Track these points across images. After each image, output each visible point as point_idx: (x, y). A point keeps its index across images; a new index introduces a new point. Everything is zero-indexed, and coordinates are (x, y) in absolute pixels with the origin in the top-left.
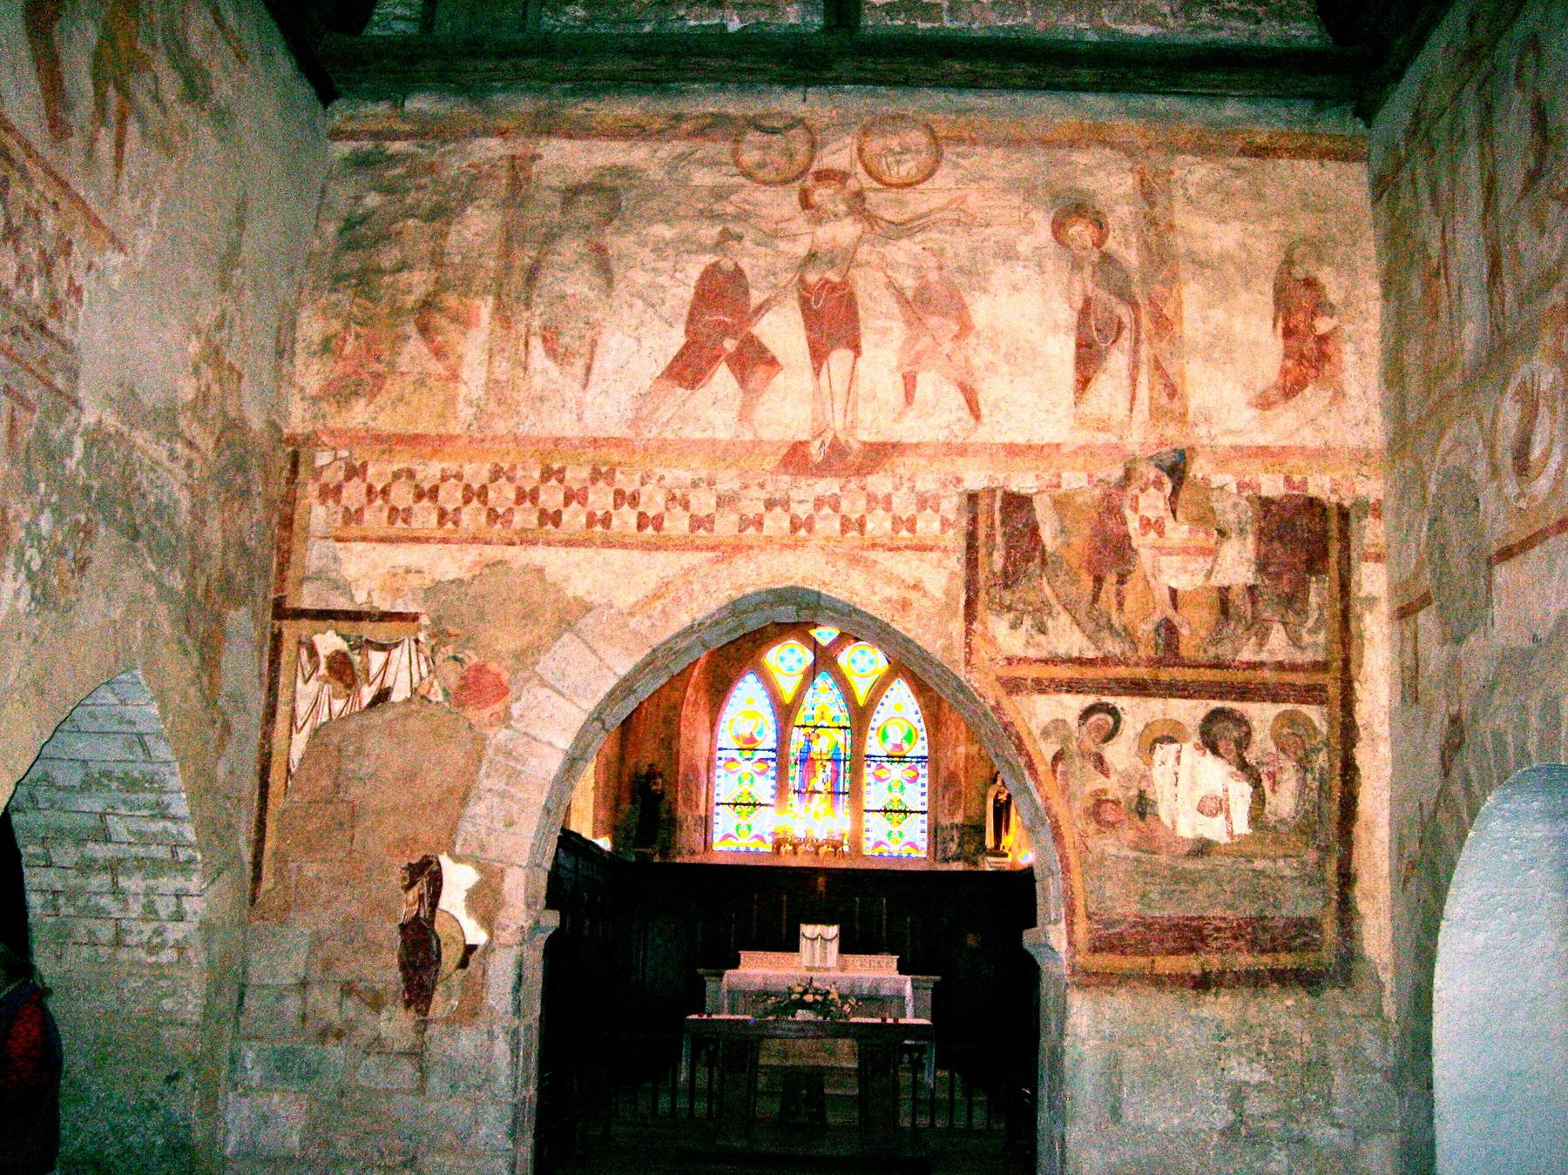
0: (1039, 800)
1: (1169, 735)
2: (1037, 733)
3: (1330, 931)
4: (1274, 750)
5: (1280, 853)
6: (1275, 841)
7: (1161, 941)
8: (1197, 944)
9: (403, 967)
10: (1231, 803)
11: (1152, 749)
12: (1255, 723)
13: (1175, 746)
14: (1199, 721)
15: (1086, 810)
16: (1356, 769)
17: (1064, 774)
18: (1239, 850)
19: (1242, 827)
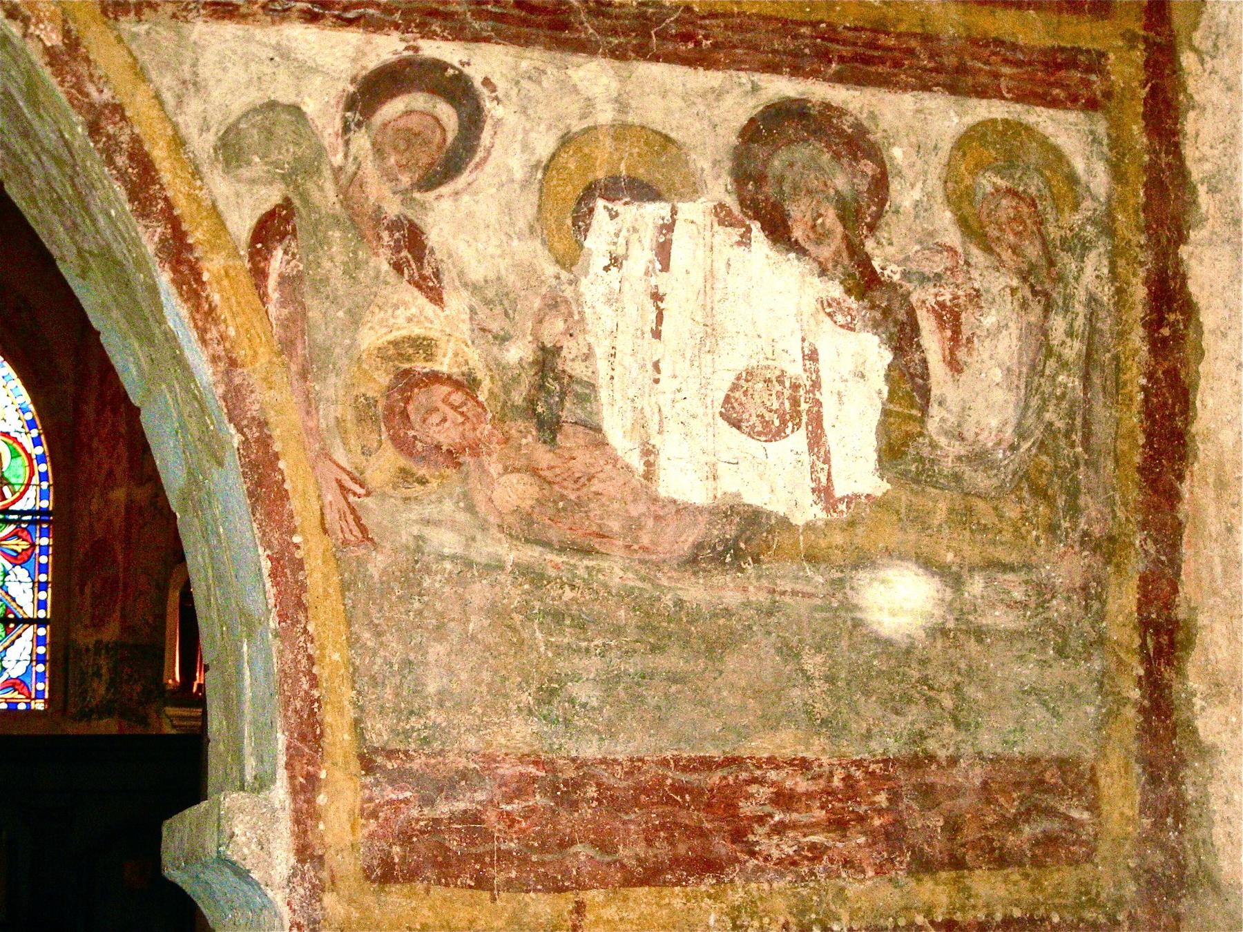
0: (205, 372)
2: (202, 144)
3: (1121, 796)
4: (953, 237)
5: (973, 554)
6: (963, 517)
7: (604, 845)
8: (721, 847)
10: (826, 397)
11: (582, 218)
13: (655, 211)
15: (364, 412)
16: (1189, 308)
17: (289, 282)
19: (858, 471)
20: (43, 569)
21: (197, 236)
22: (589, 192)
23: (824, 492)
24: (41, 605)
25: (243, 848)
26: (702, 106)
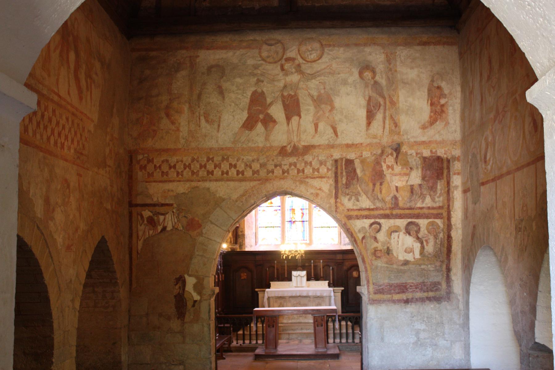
1: (396, 230)
2: (357, 231)
3: (444, 285)
4: (427, 233)
6: (428, 259)
8: (405, 290)
9: (176, 308)
11: (391, 234)
12: (421, 226)
13: (397, 233)
14: (405, 225)
16: (451, 238)
18: (417, 263)
19: (418, 256)
21: (357, 239)
22: (392, 232)
23: (414, 258)
26: (402, 223)
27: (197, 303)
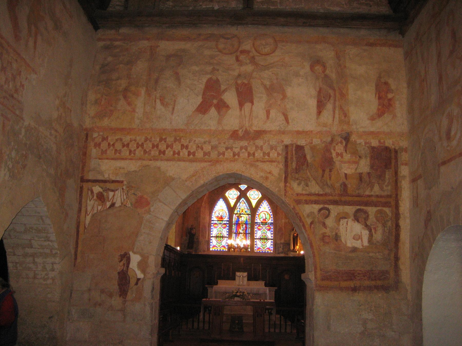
0: (306, 236)
2: (305, 216)
3: (392, 274)
4: (375, 221)
9: (119, 285)
11: (339, 221)
13: (346, 220)
16: (400, 227)
17: (313, 228)
19: (366, 243)
20: (272, 231)
23: (363, 245)
24: (272, 237)
25: (310, 276)
26: (350, 210)
27: (140, 281)
